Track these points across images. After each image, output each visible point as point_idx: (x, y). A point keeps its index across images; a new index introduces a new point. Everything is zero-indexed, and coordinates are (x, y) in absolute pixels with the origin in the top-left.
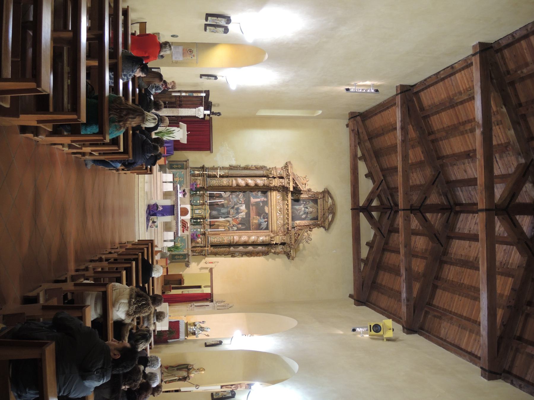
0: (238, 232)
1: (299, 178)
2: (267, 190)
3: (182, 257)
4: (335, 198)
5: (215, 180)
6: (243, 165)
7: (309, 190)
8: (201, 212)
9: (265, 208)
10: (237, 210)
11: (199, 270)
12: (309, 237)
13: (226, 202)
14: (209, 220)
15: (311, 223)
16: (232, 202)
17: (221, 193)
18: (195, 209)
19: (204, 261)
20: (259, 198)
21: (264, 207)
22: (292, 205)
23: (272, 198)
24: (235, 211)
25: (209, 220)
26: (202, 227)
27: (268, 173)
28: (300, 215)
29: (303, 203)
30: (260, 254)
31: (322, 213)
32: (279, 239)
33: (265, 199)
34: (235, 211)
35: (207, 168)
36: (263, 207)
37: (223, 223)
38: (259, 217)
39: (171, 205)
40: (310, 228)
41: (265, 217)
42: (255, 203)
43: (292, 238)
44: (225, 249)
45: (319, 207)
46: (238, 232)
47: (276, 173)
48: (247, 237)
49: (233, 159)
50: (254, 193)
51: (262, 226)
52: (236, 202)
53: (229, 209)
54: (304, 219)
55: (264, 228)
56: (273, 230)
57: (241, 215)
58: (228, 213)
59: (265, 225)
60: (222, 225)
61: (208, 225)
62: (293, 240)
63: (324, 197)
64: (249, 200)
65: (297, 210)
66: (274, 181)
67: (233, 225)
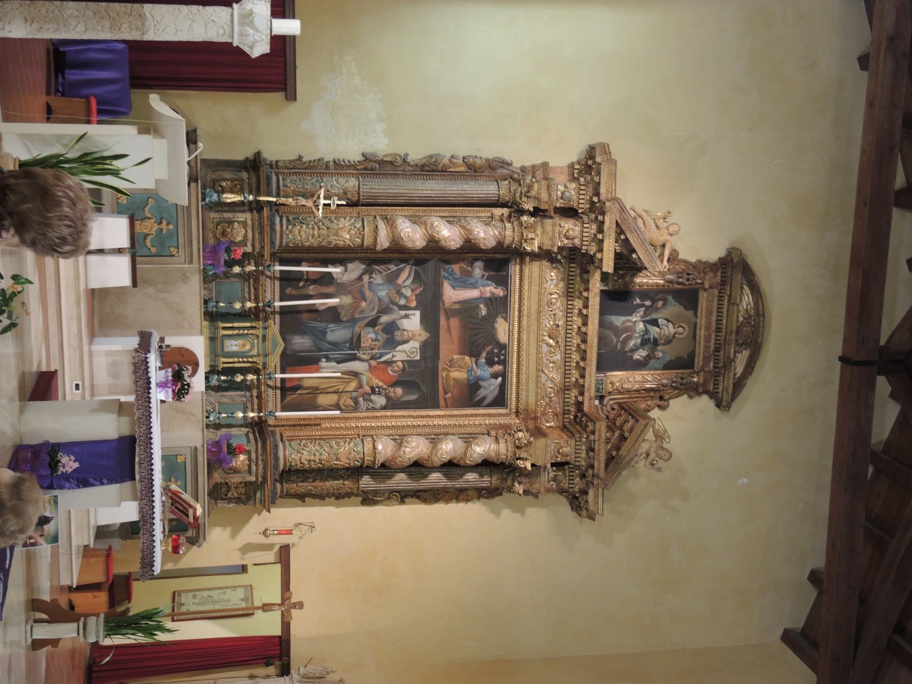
0: (389, 414)
1: (640, 222)
2: (506, 256)
4: (764, 286)
5: (308, 225)
6: (416, 155)
8: (248, 347)
9: (497, 325)
10: (387, 334)
11: (238, 554)
12: (662, 448)
13: (347, 300)
15: (665, 381)
17: (330, 273)
18: (224, 336)
20: (474, 286)
21: (494, 322)
22: (602, 312)
23: (526, 287)
24: (382, 337)
26: (252, 396)
27: (518, 195)
28: (627, 349)
29: (643, 306)
30: (469, 493)
31: (713, 341)
33: (500, 292)
34: (379, 338)
35: (271, 165)
36: (490, 320)
38: (474, 359)
39: (121, 439)
40: (661, 398)
41: (496, 359)
42: (457, 306)
43: (599, 450)
45: (702, 321)
46: (389, 414)
47: (550, 195)
48: (427, 442)
49: (380, 127)
51: (482, 393)
52: (386, 300)
53: (357, 329)
54: (640, 365)
55: (490, 399)
56: (521, 407)
57: (404, 351)
58: (355, 341)
59: (492, 388)
60: (329, 390)
61: (275, 388)
62: (603, 457)
63: (723, 283)
64: (438, 295)
65: (617, 331)
66: (539, 231)
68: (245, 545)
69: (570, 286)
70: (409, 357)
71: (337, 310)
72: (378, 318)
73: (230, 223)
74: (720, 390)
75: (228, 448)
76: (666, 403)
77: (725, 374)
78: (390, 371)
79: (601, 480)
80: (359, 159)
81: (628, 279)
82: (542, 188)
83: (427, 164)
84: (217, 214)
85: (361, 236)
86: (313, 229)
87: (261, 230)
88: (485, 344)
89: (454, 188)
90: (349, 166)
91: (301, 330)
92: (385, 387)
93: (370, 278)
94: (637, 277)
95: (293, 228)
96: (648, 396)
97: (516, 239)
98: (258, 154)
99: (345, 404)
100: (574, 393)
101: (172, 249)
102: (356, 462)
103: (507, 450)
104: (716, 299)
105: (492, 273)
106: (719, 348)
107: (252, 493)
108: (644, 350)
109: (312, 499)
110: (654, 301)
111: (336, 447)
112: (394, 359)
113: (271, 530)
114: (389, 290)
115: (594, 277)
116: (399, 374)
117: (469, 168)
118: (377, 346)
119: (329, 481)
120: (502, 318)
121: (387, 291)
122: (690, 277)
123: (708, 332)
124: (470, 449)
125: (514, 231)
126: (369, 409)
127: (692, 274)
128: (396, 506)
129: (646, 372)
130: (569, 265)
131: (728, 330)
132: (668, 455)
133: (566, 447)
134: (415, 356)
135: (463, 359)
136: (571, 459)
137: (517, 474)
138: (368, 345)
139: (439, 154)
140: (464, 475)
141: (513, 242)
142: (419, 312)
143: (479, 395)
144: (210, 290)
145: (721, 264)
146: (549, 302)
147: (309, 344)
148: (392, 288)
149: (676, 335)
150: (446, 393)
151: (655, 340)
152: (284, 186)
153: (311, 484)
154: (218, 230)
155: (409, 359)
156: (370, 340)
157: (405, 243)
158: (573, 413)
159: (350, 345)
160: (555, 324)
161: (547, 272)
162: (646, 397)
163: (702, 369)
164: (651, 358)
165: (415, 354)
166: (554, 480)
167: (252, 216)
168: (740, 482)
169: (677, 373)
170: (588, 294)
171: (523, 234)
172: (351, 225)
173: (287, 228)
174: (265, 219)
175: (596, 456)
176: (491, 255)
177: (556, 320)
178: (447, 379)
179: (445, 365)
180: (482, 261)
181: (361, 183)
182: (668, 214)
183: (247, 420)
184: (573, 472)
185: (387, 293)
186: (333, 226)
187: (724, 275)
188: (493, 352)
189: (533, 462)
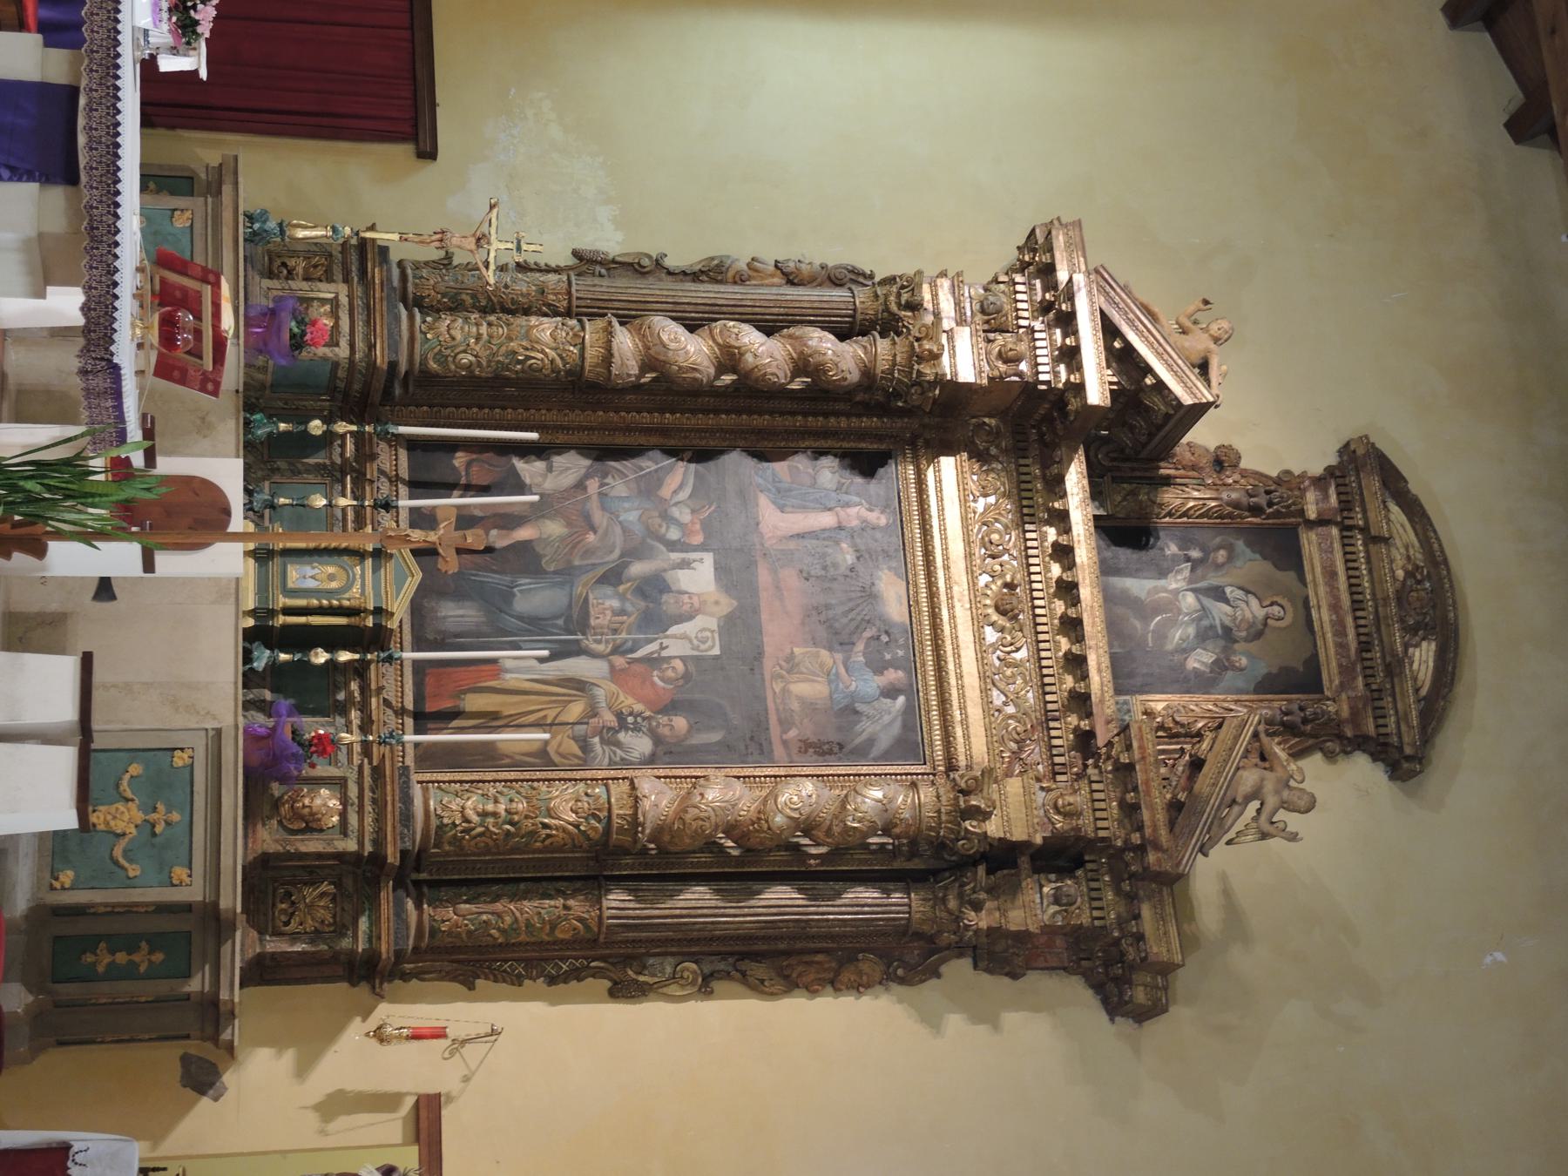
3: (158, 957)
7: (1223, 461)
8: (334, 585)
11: (313, 1119)
14: (409, 655)
16: (606, 533)
19: (355, 1033)
22: (1106, 569)
24: (635, 606)
25: (409, 655)
28: (1169, 647)
29: (1188, 559)
32: (1028, 805)
34: (629, 607)
37: (532, 703)
38: (839, 656)
43: (1147, 782)
44: (560, 902)
45: (1319, 594)
50: (780, 468)
51: (866, 728)
52: (638, 529)
53: (579, 590)
54: (1202, 683)
57: (685, 637)
59: (887, 719)
63: (1346, 505)
65: (1144, 610)
67: (620, 716)
68: (331, 1096)
70: (697, 648)
74: (1392, 727)
77: (1393, 687)
78: (656, 679)
79: (1165, 851)
81: (1143, 497)
83: (703, 269)
92: (648, 714)
93: (602, 485)
97: (898, 359)
99: (561, 750)
103: (938, 797)
104: (1337, 546)
108: (1205, 649)
112: (664, 653)
120: (890, 569)
121: (641, 511)
123: (1337, 613)
126: (616, 763)
128: (692, 1003)
134: (713, 647)
135: (817, 655)
138: (606, 622)
141: (894, 364)
147: (476, 619)
151: (1227, 630)
152: (414, 277)
153: (490, 908)
155: (696, 653)
156: (609, 613)
159: (565, 622)
160: (1006, 585)
164: (1226, 669)
165: (709, 643)
173: (424, 322)
175: (1142, 794)
179: (778, 668)
185: (641, 516)
187: (1342, 489)
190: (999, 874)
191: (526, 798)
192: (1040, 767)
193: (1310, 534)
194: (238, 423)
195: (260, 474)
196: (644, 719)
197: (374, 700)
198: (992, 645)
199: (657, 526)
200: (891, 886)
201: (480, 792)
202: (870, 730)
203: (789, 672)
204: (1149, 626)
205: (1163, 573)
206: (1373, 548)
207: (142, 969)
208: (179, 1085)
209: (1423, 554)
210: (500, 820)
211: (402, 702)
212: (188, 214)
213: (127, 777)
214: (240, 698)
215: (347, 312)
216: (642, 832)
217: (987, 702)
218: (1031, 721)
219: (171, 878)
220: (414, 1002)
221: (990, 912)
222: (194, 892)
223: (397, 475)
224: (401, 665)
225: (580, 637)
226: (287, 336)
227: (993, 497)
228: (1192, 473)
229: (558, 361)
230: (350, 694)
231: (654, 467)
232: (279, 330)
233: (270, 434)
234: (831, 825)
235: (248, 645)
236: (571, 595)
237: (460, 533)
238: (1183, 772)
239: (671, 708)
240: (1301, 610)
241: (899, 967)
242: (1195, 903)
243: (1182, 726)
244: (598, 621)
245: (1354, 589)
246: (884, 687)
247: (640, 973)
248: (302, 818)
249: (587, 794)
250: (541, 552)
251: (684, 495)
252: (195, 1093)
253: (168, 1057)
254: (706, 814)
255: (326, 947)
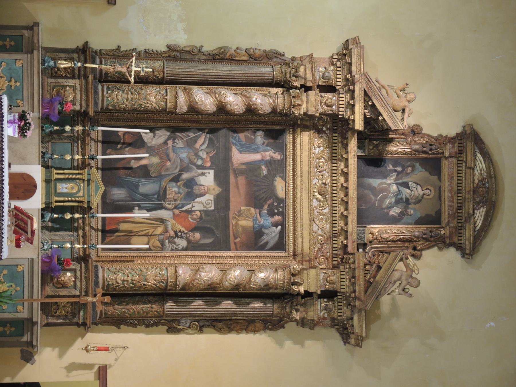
0: (189, 254)
1: (384, 92)
3: (13, 329)
4: (496, 157)
6: (209, 47)
8: (75, 191)
9: (276, 183)
11: (64, 371)
13: (155, 160)
14: (100, 215)
17: (139, 133)
19: (80, 343)
20: (257, 151)
21: (273, 180)
22: (361, 175)
23: (298, 153)
24: (184, 190)
25: (100, 215)
26: (78, 236)
28: (384, 206)
29: (396, 171)
31: (455, 201)
33: (277, 156)
34: (181, 191)
35: (96, 52)
36: (270, 179)
38: (258, 211)
41: (276, 211)
42: (244, 167)
43: (359, 276)
45: (445, 185)
46: (189, 254)
47: (313, 75)
49: (181, 26)
51: (265, 239)
52: (187, 161)
53: (163, 184)
54: (395, 220)
55: (271, 244)
56: (299, 250)
58: (162, 193)
59: (273, 235)
63: (460, 152)
64: (228, 158)
65: (375, 191)
67: (176, 233)
69: (334, 151)
70: (205, 207)
71: (147, 168)
72: (180, 175)
73: (64, 87)
75: (58, 261)
76: (419, 253)
80: (164, 50)
81: (381, 147)
82: (307, 70)
84: (53, 79)
85: (165, 100)
86: (127, 94)
87: (87, 92)
88: (266, 198)
89: (238, 69)
90: (156, 54)
91: (119, 185)
92: (186, 232)
93: (174, 143)
94: (389, 146)
95: (111, 93)
96: (404, 247)
97: (286, 106)
98: (86, 44)
99: (154, 245)
100: (342, 238)
101: (18, 101)
102: (161, 284)
103: (284, 276)
105: (271, 141)
106: (461, 206)
107: (76, 312)
109: (126, 327)
110: (404, 168)
111: (145, 270)
112: (193, 209)
113: (92, 346)
114: (189, 153)
115: (352, 141)
116: (197, 221)
117: (250, 57)
118: (179, 198)
119: (139, 304)
120: (280, 177)
121: (187, 154)
122: (432, 147)
123: (451, 193)
124: (254, 275)
125: (285, 99)
126: (173, 250)
127: (434, 145)
128: (196, 335)
129: (401, 226)
130: (332, 135)
131: (467, 190)
132: (416, 282)
133: (333, 276)
134: (210, 207)
135: (249, 210)
136: (337, 287)
137: (295, 304)
138: (172, 197)
139: (227, 47)
140: (250, 303)
142: (213, 170)
143: (262, 241)
144: (47, 148)
145: (458, 137)
146: (318, 165)
147: (125, 195)
148: (191, 151)
149: (424, 196)
150: (235, 238)
151: (407, 199)
153: (126, 307)
154: (54, 92)
156: (174, 193)
157: (199, 106)
158: (341, 256)
160: (323, 183)
161: (315, 141)
162: (402, 247)
163: (448, 224)
164: (404, 215)
165: (210, 205)
166: (326, 309)
167: (80, 81)
168: (488, 325)
169: (427, 228)
170: (348, 156)
171: (291, 101)
172: (157, 92)
173: (108, 93)
174: (90, 83)
175: (356, 280)
176: (270, 126)
177: (323, 180)
178: (236, 226)
179: (235, 215)
180: (263, 131)
181: (165, 65)
182: (406, 86)
183: (74, 255)
184: (341, 302)
185: (188, 155)
186: (143, 92)
187: (460, 145)
188: (273, 204)
189: (306, 289)
190: (306, 299)
191: (138, 275)
192: (328, 254)
193: (445, 161)
194: (39, 131)
195: (47, 139)
196: (184, 234)
197: (87, 228)
198: (316, 207)
199: (193, 159)
200: (267, 301)
201: (122, 272)
202: (267, 239)
203: (239, 216)
204: (377, 198)
205: (385, 177)
206: (468, 171)
207: (8, 333)
208: (20, 359)
209: (487, 173)
210: (129, 283)
211: (98, 227)
212: (21, 61)
213: (2, 274)
214: (40, 225)
215: (79, 91)
216: (178, 288)
217: (311, 230)
218: (327, 236)
219: (17, 309)
220: (99, 333)
221: (301, 312)
222: (24, 314)
223: (97, 139)
224: (98, 219)
225: (163, 202)
226: (56, 112)
227: (322, 148)
228: (403, 136)
229: (157, 107)
230: (79, 224)
231: (194, 135)
232: (54, 109)
233: (51, 131)
234: (245, 285)
235: (43, 212)
236: (160, 186)
237: (103, 297)
238: (375, 268)
239: (195, 229)
240: (438, 192)
241: (270, 325)
242: (381, 303)
243: (384, 239)
244: (169, 196)
245: (459, 185)
246: (274, 223)
247: (178, 325)
248: (61, 284)
249: (159, 273)
250: (150, 169)
251: (204, 147)
252: (25, 362)
253: (16, 351)
254: (201, 282)
255: (69, 321)
